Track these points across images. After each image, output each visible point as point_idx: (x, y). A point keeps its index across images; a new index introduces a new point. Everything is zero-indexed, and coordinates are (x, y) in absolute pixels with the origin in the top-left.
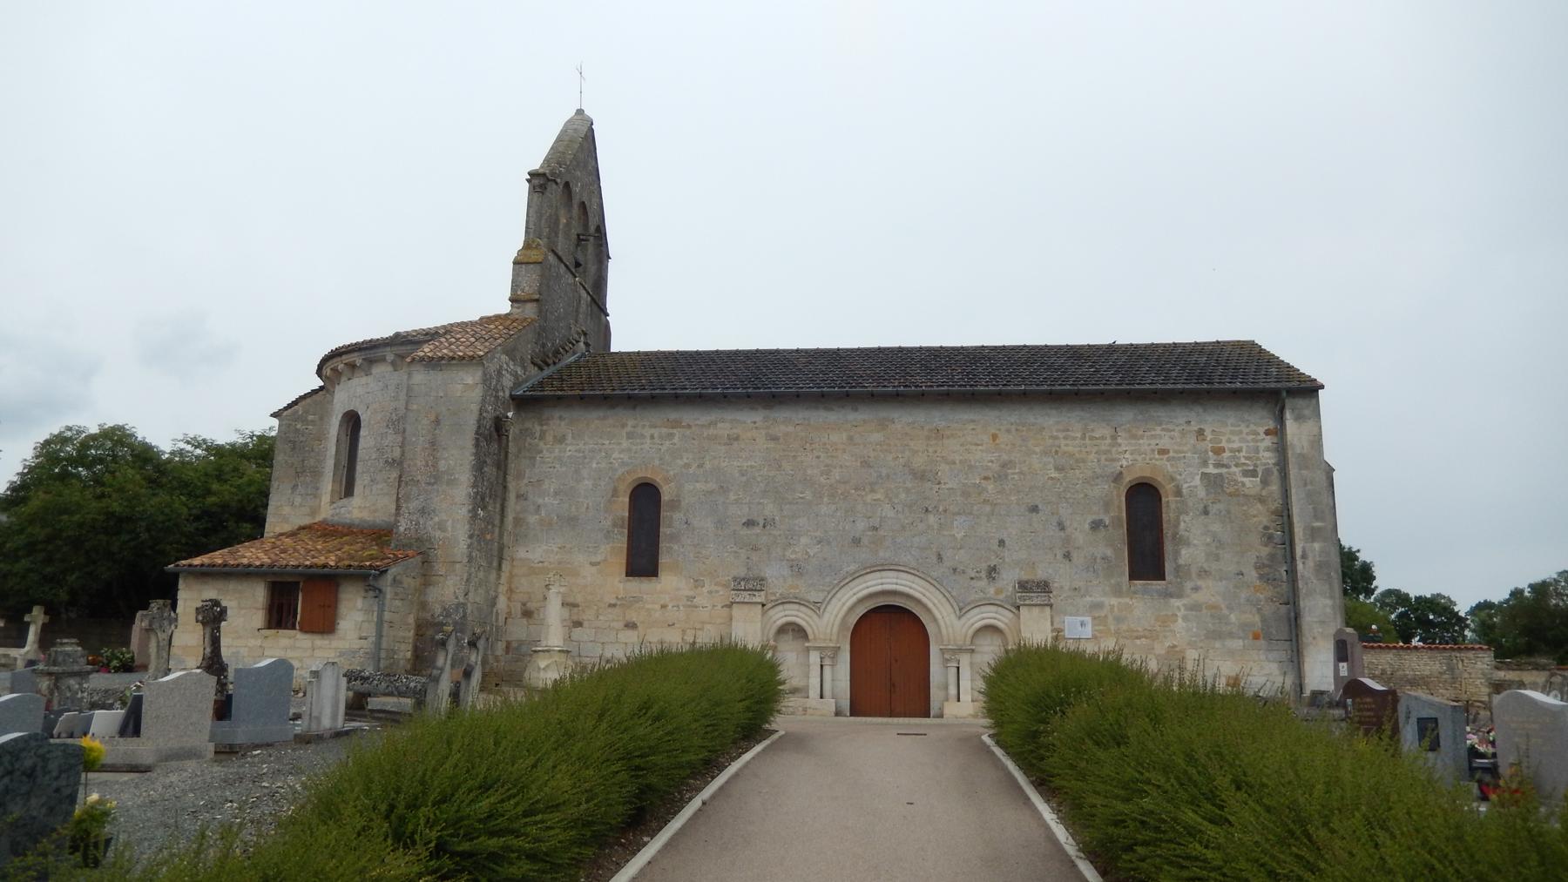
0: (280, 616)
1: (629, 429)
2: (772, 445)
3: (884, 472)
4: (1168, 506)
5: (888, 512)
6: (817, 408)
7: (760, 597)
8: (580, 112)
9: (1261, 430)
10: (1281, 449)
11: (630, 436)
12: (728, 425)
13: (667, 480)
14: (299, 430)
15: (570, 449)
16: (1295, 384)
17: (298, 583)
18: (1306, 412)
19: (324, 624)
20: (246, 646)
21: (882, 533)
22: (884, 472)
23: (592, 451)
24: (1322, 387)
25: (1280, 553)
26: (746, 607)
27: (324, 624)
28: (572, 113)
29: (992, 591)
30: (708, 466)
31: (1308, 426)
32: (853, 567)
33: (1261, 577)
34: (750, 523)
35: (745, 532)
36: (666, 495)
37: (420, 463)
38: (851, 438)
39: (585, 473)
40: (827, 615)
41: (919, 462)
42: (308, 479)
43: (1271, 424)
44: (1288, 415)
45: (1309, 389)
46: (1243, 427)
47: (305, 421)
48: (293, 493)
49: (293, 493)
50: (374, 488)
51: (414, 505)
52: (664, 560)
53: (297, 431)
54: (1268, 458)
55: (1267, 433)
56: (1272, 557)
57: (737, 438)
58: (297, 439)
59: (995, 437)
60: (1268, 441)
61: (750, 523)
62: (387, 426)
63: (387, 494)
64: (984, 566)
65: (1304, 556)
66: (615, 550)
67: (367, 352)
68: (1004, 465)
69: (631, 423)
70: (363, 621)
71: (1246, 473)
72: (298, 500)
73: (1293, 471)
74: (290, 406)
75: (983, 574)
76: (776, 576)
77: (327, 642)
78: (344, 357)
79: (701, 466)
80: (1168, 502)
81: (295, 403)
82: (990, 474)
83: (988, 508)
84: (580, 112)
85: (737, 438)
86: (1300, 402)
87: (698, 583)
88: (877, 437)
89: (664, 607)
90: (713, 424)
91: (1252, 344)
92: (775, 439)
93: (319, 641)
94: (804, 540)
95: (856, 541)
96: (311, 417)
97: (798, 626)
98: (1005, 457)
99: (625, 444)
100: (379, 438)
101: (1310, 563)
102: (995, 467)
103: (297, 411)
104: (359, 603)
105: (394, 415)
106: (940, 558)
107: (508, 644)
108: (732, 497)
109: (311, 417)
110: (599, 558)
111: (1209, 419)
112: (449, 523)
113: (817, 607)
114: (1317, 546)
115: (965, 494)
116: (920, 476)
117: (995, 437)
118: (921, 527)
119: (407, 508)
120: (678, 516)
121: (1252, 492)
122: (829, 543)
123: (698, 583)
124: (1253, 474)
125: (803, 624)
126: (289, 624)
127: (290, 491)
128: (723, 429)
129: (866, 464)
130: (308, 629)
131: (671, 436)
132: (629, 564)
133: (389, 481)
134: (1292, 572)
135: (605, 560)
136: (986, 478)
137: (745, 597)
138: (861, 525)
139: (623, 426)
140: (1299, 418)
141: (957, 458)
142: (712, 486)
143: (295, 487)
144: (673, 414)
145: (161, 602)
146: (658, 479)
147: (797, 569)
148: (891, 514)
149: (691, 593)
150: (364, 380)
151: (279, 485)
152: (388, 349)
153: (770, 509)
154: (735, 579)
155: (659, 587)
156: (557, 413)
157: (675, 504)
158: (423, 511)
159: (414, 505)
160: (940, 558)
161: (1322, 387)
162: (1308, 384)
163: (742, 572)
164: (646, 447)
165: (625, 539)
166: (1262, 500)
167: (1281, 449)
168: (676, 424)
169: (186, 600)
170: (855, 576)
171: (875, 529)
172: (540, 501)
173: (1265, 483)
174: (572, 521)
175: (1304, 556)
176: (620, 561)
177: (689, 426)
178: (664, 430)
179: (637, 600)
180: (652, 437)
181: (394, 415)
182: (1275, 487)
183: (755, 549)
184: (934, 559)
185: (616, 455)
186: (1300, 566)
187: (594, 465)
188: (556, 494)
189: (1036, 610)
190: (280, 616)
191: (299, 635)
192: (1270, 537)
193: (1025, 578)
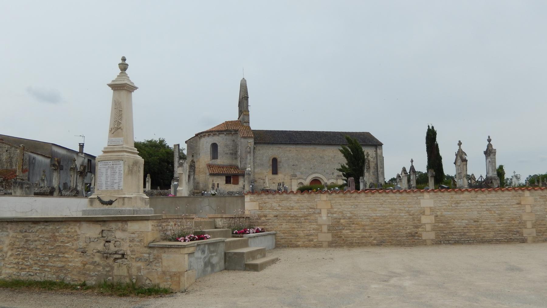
0: (228, 181)
1: (272, 148)
2: (297, 152)
3: (315, 157)
5: (316, 163)
7: (296, 178)
8: (244, 79)
9: (374, 151)
10: (376, 154)
11: (272, 149)
12: (289, 148)
13: (279, 158)
15: (261, 152)
16: (379, 144)
17: (231, 176)
18: (381, 148)
19: (236, 183)
21: (315, 167)
22: (315, 157)
23: (265, 152)
24: (383, 144)
25: (376, 170)
26: (294, 180)
27: (236, 183)
28: (242, 78)
29: (333, 176)
30: (286, 155)
31: (381, 151)
32: (311, 173)
33: (373, 174)
34: (293, 165)
35: (293, 167)
36: (279, 160)
37: (244, 155)
38: (310, 151)
39: (264, 156)
40: (307, 181)
41: (321, 155)
43: (375, 150)
44: (378, 149)
45: (381, 145)
46: (371, 150)
47: (193, 143)
51: (243, 163)
52: (279, 171)
53: (191, 145)
54: (374, 155)
55: (374, 151)
56: (375, 171)
57: (291, 150)
59: (333, 151)
60: (374, 153)
61: (293, 165)
64: (332, 172)
65: (379, 171)
66: (270, 170)
68: (335, 156)
69: (272, 147)
71: (371, 158)
73: (378, 158)
74: (189, 140)
75: (331, 174)
76: (298, 174)
79: (284, 155)
81: (190, 139)
82: (332, 157)
83: (332, 163)
84: (244, 79)
85: (291, 150)
86: (379, 147)
87: (285, 176)
88: (314, 151)
89: (279, 180)
90: (286, 148)
91: (369, 133)
92: (297, 151)
93: (236, 186)
94: (303, 168)
95: (311, 168)
96: (194, 142)
97: (301, 182)
98: (335, 155)
99: (271, 151)
101: (380, 172)
102: (333, 156)
104: (242, 179)
106: (325, 171)
107: (195, 189)
108: (290, 161)
109: (194, 142)
110: (267, 171)
111: (366, 149)
113: (305, 180)
114: (381, 169)
115: (329, 161)
116: (321, 157)
117: (333, 151)
118: (322, 166)
120: (281, 164)
121: (372, 161)
122: (307, 169)
123: (285, 176)
124: (372, 158)
125: (302, 182)
128: (288, 149)
129: (312, 155)
130: (234, 183)
131: (279, 150)
132: (272, 172)
134: (378, 174)
135: (269, 172)
137: (294, 178)
138: (312, 166)
139: (271, 148)
140: (379, 149)
141: (327, 154)
142: (287, 159)
144: (279, 146)
145: (353, 179)
146: (277, 157)
147: (302, 173)
148: (317, 164)
149: (284, 177)
150: (217, 137)
153: (297, 163)
154: (292, 175)
155: (278, 176)
156: (258, 145)
157: (280, 162)
158: (245, 164)
159: (243, 163)
160: (325, 171)
161: (383, 144)
162: (381, 144)
163: (293, 174)
164: (275, 152)
165: (271, 168)
166: (373, 162)
167: (376, 154)
168: (280, 148)
170: (311, 174)
171: (314, 166)
172: (256, 161)
173: (374, 159)
174: (262, 165)
175: (379, 171)
176: (271, 173)
177: (282, 148)
178: (278, 149)
179: (275, 178)
180: (276, 150)
182: (375, 160)
183: (294, 170)
184: (324, 171)
185: (269, 153)
186: (379, 173)
187: (266, 155)
188: (259, 160)
189: (340, 180)
190: (228, 181)
191: (232, 185)
192: (374, 168)
193: (338, 174)
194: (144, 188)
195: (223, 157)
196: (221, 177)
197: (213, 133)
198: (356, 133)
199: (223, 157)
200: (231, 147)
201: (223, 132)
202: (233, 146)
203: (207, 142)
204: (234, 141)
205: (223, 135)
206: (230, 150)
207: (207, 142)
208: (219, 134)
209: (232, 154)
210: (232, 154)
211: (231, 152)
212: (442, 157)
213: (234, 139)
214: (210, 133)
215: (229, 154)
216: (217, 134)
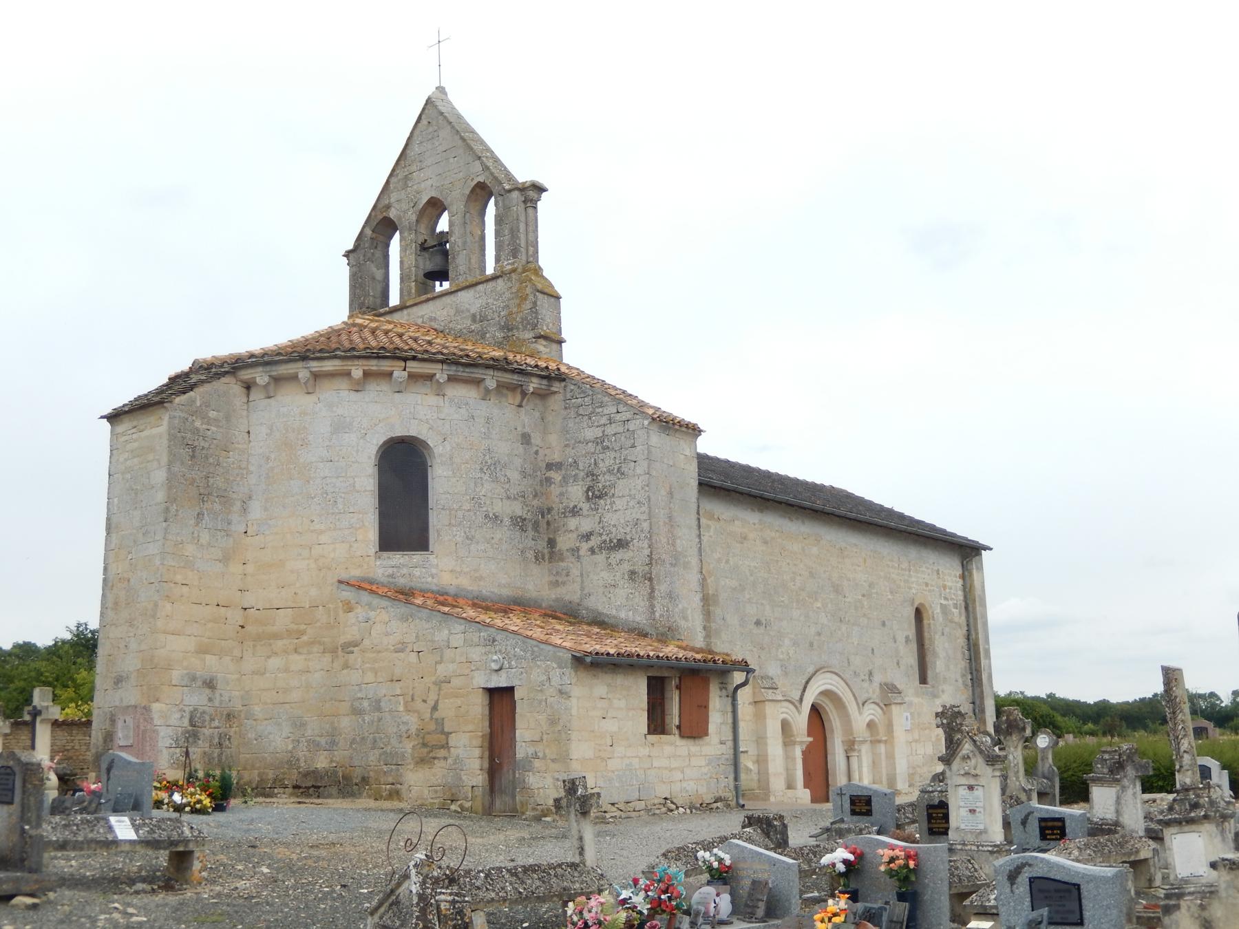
4: (930, 627)
6: (785, 517)
14: (197, 429)
20: (636, 757)
42: (217, 507)
47: (205, 417)
48: (197, 525)
49: (197, 525)
50: (473, 547)
58: (196, 443)
62: (481, 469)
63: (494, 559)
67: (461, 369)
70: (721, 724)
72: (205, 537)
77: (698, 748)
78: (410, 364)
79: (727, 562)
80: (929, 624)
96: (212, 414)
100: (472, 485)
103: (194, 401)
105: (487, 457)
109: (212, 414)
112: (689, 611)
119: (659, 591)
126: (659, 730)
127: (192, 522)
133: (493, 542)
136: (863, 596)
143: (200, 516)
150: (433, 400)
151: (177, 510)
152: (491, 372)
169: (578, 698)
181: (487, 457)
191: (679, 742)
194: (943, 806)
195: (470, 538)
196: (620, 680)
197: (413, 366)
198: (796, 483)
199: (470, 538)
200: (515, 476)
201: (478, 373)
202: (524, 474)
203: (340, 427)
204: (526, 439)
205: (466, 393)
206: (508, 498)
207: (340, 427)
208: (451, 379)
209: (519, 523)
210: (519, 523)
211: (517, 509)
212: (27, 640)
213: (527, 430)
214: (385, 365)
215: (507, 521)
216: (441, 377)
